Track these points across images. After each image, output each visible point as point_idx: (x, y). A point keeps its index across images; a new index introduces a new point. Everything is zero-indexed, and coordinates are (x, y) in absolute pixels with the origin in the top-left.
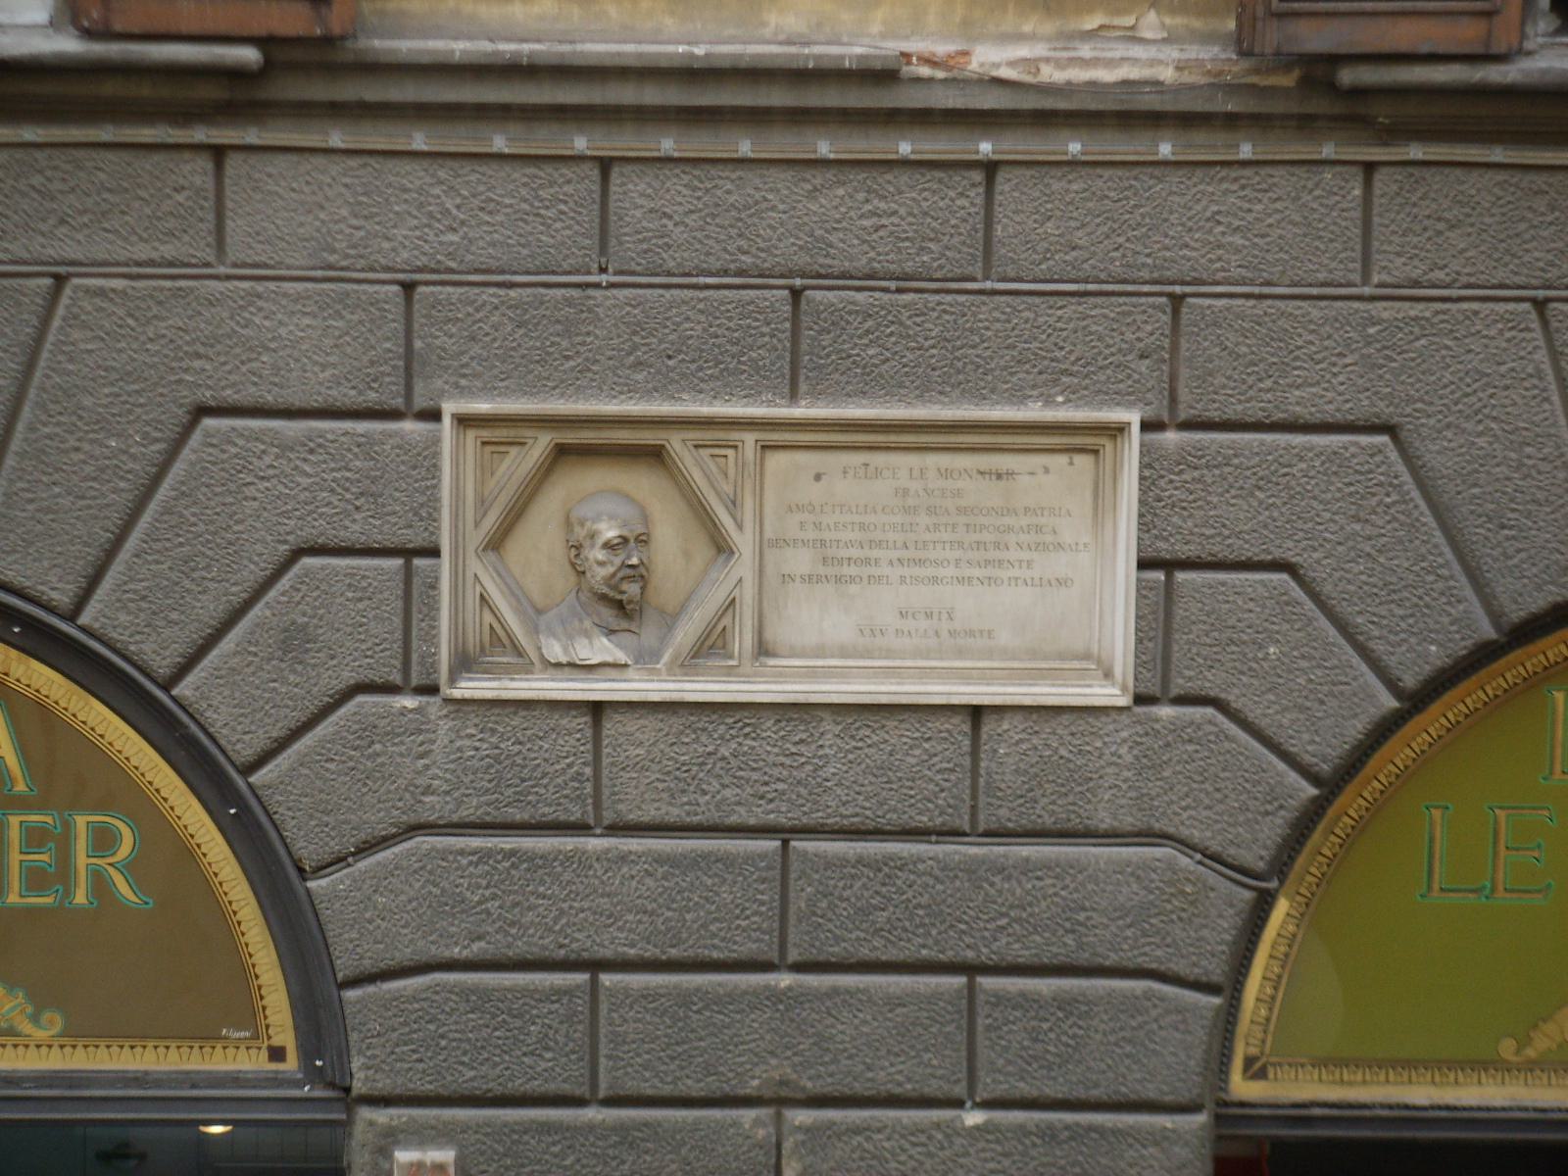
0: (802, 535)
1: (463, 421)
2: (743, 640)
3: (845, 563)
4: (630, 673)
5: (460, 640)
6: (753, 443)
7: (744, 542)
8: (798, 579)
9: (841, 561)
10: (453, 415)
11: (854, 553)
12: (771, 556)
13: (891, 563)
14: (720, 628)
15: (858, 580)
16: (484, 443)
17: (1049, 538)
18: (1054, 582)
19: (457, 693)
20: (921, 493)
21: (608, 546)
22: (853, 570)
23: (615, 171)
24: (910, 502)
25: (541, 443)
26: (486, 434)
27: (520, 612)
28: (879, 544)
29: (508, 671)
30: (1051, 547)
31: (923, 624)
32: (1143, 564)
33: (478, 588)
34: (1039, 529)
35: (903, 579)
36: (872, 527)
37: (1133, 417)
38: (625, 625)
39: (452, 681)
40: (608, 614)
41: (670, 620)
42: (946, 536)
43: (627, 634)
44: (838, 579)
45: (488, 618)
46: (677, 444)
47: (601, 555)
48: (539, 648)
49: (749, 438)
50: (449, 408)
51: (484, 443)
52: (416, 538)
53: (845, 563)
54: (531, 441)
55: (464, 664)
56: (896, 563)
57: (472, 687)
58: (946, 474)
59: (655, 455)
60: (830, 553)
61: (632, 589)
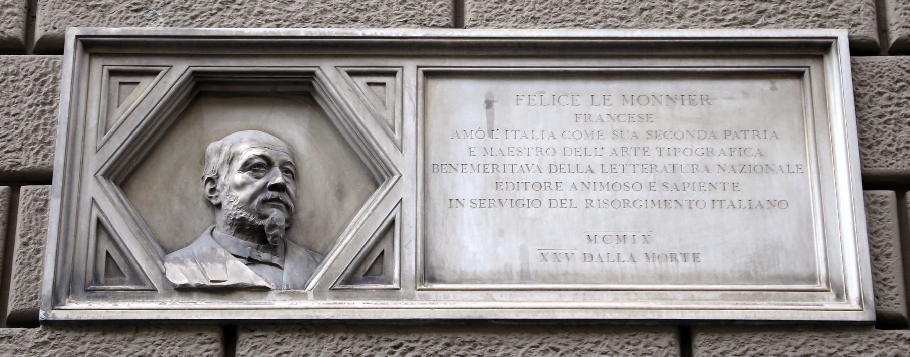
0: (470, 160)
1: (91, 47)
2: (404, 260)
3: (522, 186)
4: (271, 295)
5: (69, 260)
6: (414, 69)
7: (405, 163)
8: (468, 204)
9: (516, 186)
10: (77, 37)
11: (531, 177)
12: (436, 181)
13: (574, 186)
14: (377, 253)
15: (536, 204)
16: (112, 73)
17: (756, 161)
18: (766, 205)
19: (60, 315)
20: (605, 118)
21: (247, 167)
22: (530, 194)
23: (243, 337)
24: (596, 127)
25: (176, 73)
26: (116, 63)
27: (147, 248)
28: (559, 168)
29: (128, 295)
30: (759, 169)
31: (613, 247)
32: (870, 182)
33: (95, 212)
34: (742, 151)
35: (589, 202)
36: (550, 152)
37: (842, 36)
38: (265, 256)
39: (56, 301)
40: (246, 246)
41: (317, 255)
42: (635, 160)
43: (268, 268)
44: (516, 203)
45: (105, 246)
46: (330, 74)
47: (239, 178)
48: (164, 274)
49: (410, 69)
50: (71, 34)
51: (112, 73)
52: (28, 161)
53: (522, 186)
54: (165, 69)
55: (68, 285)
56: (579, 186)
57: (79, 308)
58: (635, 99)
59: (300, 92)
60: (503, 177)
61: (276, 215)
